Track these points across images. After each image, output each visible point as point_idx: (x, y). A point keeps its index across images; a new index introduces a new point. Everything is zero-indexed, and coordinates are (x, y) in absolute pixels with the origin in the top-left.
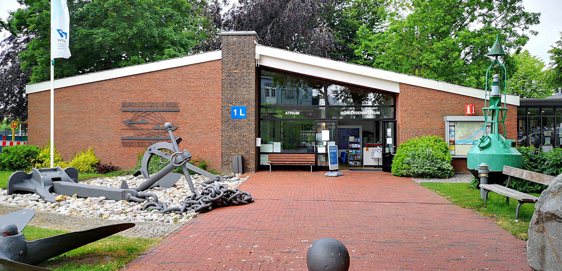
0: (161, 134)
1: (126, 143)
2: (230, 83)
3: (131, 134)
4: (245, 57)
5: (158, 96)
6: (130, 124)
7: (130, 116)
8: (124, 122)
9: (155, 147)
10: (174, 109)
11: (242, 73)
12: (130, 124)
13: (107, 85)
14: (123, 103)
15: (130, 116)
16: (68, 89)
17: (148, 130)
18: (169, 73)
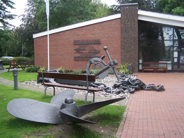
0: (96, 53)
1: (76, 59)
2: (124, 31)
3: (78, 55)
4: (133, 16)
5: (90, 37)
6: (78, 51)
7: (77, 47)
8: (75, 50)
9: (93, 60)
10: (98, 43)
11: (131, 24)
12: (78, 51)
13: (67, 33)
14: (74, 41)
15: (77, 47)
16: (40, 38)
17: (86, 53)
18: (95, 26)
